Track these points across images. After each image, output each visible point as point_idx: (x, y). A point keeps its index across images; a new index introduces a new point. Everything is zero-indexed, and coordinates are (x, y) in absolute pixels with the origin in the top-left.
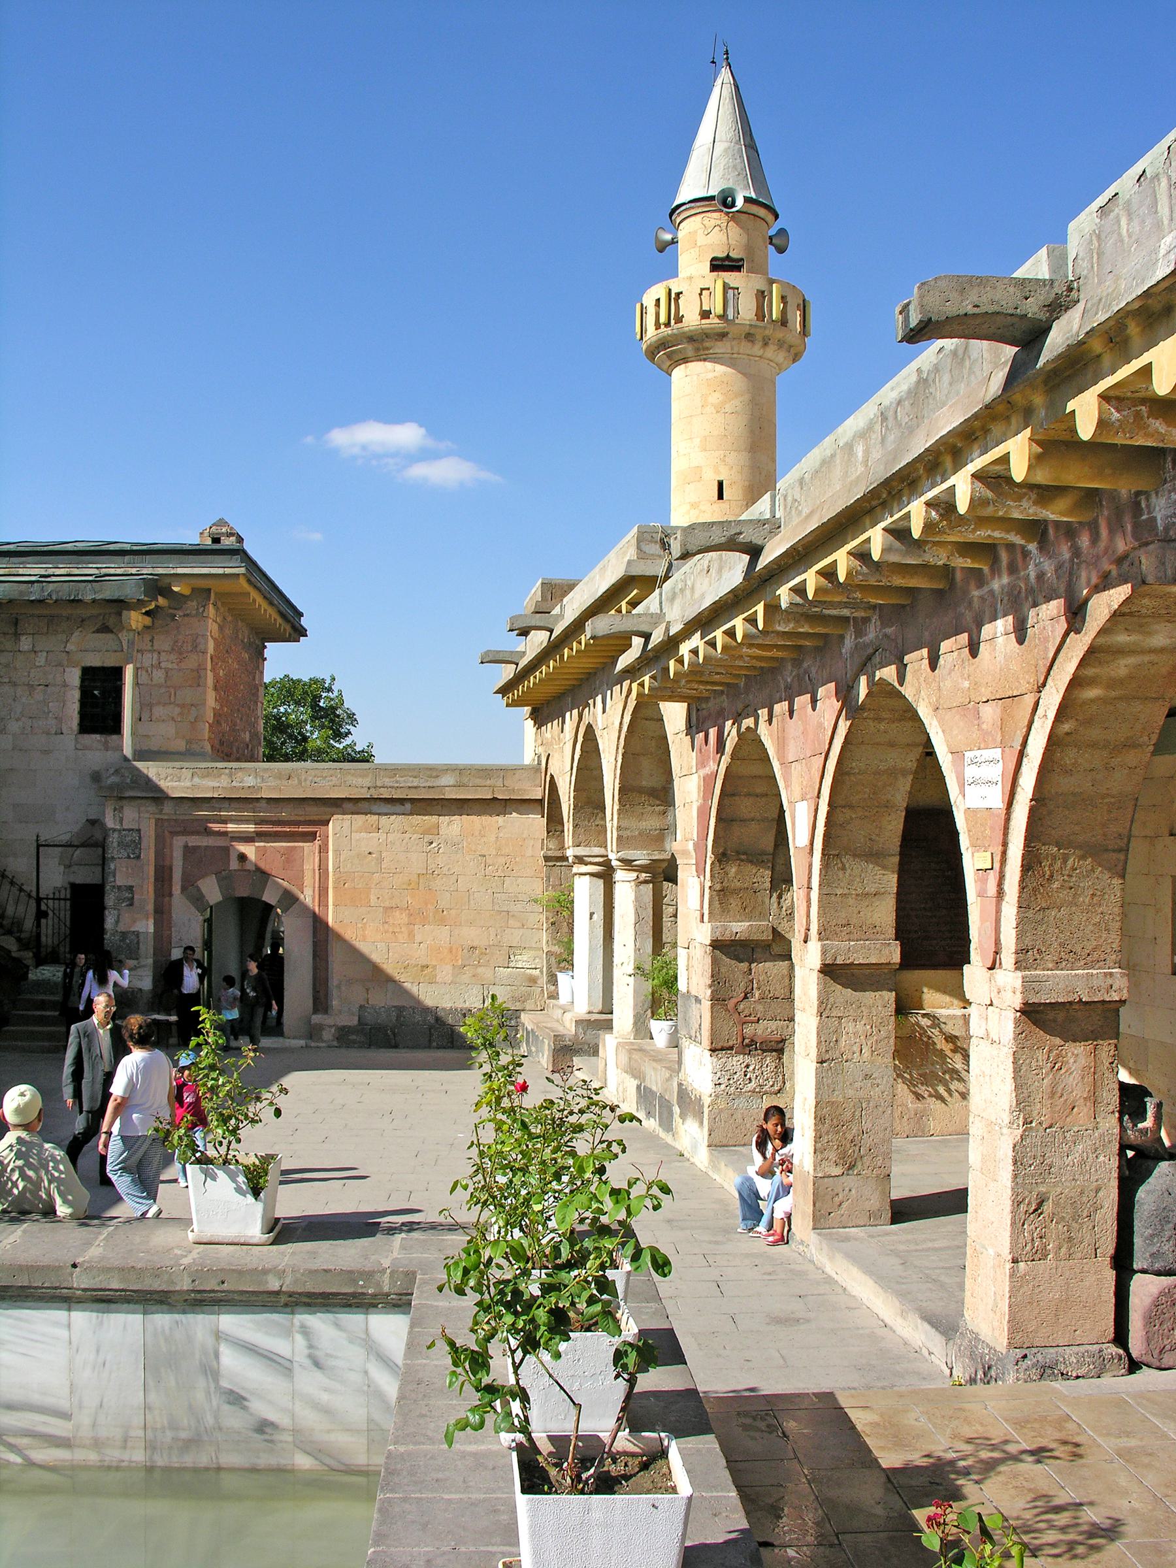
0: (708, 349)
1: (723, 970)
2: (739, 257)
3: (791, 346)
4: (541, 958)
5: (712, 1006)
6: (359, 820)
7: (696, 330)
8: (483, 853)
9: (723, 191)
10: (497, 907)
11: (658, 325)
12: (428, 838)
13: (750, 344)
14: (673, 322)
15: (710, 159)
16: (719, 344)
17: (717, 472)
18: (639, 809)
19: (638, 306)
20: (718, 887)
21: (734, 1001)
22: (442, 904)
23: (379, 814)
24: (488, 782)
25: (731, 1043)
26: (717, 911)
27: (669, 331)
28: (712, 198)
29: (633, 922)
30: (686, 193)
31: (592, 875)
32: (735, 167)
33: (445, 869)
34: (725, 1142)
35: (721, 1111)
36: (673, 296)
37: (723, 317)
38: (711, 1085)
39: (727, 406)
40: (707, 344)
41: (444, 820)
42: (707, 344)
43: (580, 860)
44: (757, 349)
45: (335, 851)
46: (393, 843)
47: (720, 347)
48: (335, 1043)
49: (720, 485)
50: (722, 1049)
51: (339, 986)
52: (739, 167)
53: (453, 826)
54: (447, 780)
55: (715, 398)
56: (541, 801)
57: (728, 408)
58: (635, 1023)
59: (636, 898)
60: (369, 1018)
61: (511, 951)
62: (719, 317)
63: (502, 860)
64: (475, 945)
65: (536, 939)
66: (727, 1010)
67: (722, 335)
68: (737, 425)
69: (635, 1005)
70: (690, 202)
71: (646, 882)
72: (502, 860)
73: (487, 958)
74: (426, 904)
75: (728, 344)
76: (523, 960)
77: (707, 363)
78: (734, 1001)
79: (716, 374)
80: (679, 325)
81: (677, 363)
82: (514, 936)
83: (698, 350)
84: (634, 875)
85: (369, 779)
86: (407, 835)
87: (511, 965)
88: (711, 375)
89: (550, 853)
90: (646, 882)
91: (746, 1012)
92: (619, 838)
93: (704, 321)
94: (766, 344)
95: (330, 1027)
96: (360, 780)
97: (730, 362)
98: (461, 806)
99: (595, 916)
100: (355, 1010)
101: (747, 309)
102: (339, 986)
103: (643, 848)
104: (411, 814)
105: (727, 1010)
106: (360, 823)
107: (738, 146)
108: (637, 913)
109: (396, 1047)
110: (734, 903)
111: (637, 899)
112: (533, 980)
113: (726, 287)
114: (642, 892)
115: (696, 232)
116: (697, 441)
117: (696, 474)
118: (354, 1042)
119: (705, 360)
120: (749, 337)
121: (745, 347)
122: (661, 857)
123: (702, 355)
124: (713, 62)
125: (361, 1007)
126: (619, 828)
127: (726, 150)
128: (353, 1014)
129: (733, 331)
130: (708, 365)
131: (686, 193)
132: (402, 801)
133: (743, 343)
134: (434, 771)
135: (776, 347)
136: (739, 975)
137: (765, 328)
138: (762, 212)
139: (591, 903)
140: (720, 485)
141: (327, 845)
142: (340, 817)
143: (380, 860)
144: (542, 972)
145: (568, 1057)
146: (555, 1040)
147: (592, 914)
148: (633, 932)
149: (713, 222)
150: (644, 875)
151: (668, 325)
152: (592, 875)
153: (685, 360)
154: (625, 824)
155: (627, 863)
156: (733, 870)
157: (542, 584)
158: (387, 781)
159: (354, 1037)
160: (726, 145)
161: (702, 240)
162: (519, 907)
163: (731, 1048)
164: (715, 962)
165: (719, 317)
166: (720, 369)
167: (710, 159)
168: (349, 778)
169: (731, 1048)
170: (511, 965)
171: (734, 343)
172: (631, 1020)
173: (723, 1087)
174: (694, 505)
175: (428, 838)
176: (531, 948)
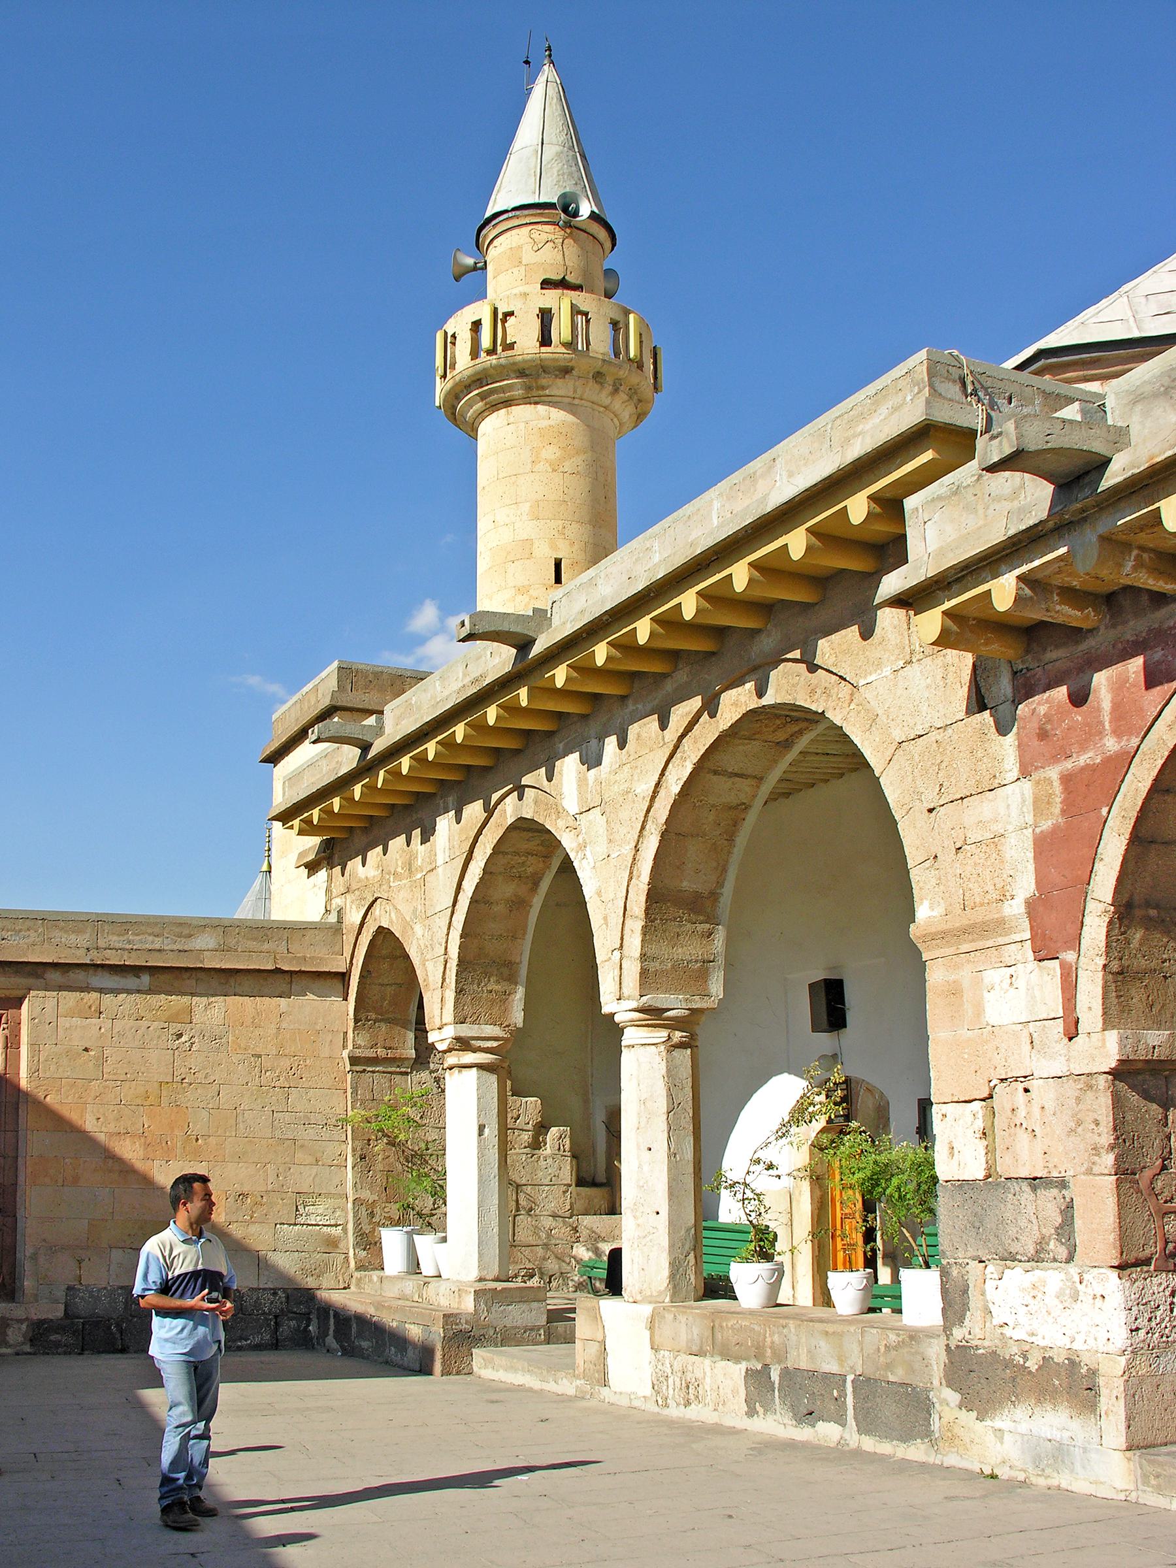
0: (543, 388)
1: (1129, 1117)
2: (578, 282)
3: (640, 401)
4: (344, 1210)
5: (1119, 1184)
6: (70, 999)
7: (533, 360)
8: (258, 1051)
9: (564, 196)
10: (278, 1134)
11: (475, 354)
12: (175, 1028)
13: (597, 387)
14: (499, 349)
15: (534, 157)
16: (559, 382)
17: (554, 547)
18: (673, 927)
19: (439, 336)
20: (1115, 966)
21: (1148, 1174)
22: (196, 1129)
23: (101, 991)
24: (266, 946)
25: (1147, 1252)
26: (1114, 1011)
27: (493, 359)
28: (551, 206)
29: (665, 1110)
30: (501, 200)
31: (480, 1067)
32: (571, 174)
33: (200, 1075)
34: (1150, 1440)
35: (1142, 1380)
36: (500, 316)
37: (570, 345)
38: (1124, 1333)
39: (567, 464)
40: (543, 382)
41: (200, 1002)
42: (543, 382)
43: (463, 1044)
44: (604, 397)
45: (32, 1045)
46: (121, 1035)
47: (561, 388)
48: (27, 1348)
49: (558, 565)
50: (1135, 1265)
51: (34, 1257)
52: (576, 175)
53: (211, 1011)
54: (205, 941)
55: (551, 453)
56: (344, 977)
57: (568, 466)
58: (672, 1276)
59: (668, 1070)
60: (82, 1306)
61: (301, 1200)
62: (565, 345)
63: (285, 1063)
64: (245, 1190)
65: (336, 1181)
66: (1139, 1191)
67: (566, 371)
68: (578, 488)
69: (672, 1246)
70: (514, 209)
71: (681, 1045)
72: (285, 1063)
73: (265, 1209)
74: (172, 1129)
75: (571, 384)
76: (317, 1213)
77: (539, 407)
78: (1148, 1174)
79: (551, 422)
80: (510, 353)
81: (494, 407)
82: (304, 1178)
83: (529, 388)
84: (663, 1034)
85: (87, 936)
86: (144, 1023)
87: (301, 1220)
88: (545, 423)
89: (358, 1053)
90: (681, 1045)
91: (1167, 1194)
92: (644, 973)
93: (544, 349)
94: (616, 391)
95: (20, 1321)
96: (73, 937)
97: (571, 409)
98: (226, 980)
99: (487, 1131)
100: (60, 1294)
101: (600, 340)
102: (34, 1257)
103: (677, 991)
104: (150, 991)
105: (1139, 1191)
106: (72, 1003)
107: (571, 153)
108: (670, 1096)
109: (123, 1350)
110: (1137, 996)
111: (671, 1073)
112: (332, 1244)
113: (575, 311)
114: (678, 1062)
115: (520, 247)
116: (526, 507)
117: (526, 548)
118: (57, 1344)
119: (536, 403)
120: (598, 376)
121: (591, 391)
122: (704, 1005)
123: (532, 397)
124: (527, 62)
125: (70, 1288)
126: (643, 957)
127: (559, 154)
128: (57, 1302)
129: (582, 366)
130: (541, 408)
131: (501, 200)
132: (136, 970)
133: (591, 383)
134: (185, 928)
135: (625, 397)
136: (1151, 1127)
137: (620, 367)
138: (602, 234)
139: (479, 1110)
140: (558, 565)
141: (17, 1035)
142: (41, 993)
143: (102, 1060)
144: (345, 1230)
145: (464, 1349)
146: (445, 1324)
147: (481, 1129)
148: (665, 1127)
149: (544, 237)
150: (678, 1034)
151: (492, 352)
152: (480, 1067)
153: (507, 403)
154: (653, 950)
155: (653, 1015)
156: (1138, 936)
157: (339, 668)
158: (115, 941)
159: (58, 1337)
160: (558, 149)
161: (529, 256)
162: (311, 1133)
163: (1147, 1262)
164: (1118, 1103)
165: (565, 345)
166: (558, 416)
167: (534, 157)
168: (57, 933)
169: (1147, 1262)
170: (301, 1220)
171: (581, 382)
172: (665, 1272)
173: (1142, 1333)
174: (521, 590)
175: (175, 1028)
176: (329, 1195)
